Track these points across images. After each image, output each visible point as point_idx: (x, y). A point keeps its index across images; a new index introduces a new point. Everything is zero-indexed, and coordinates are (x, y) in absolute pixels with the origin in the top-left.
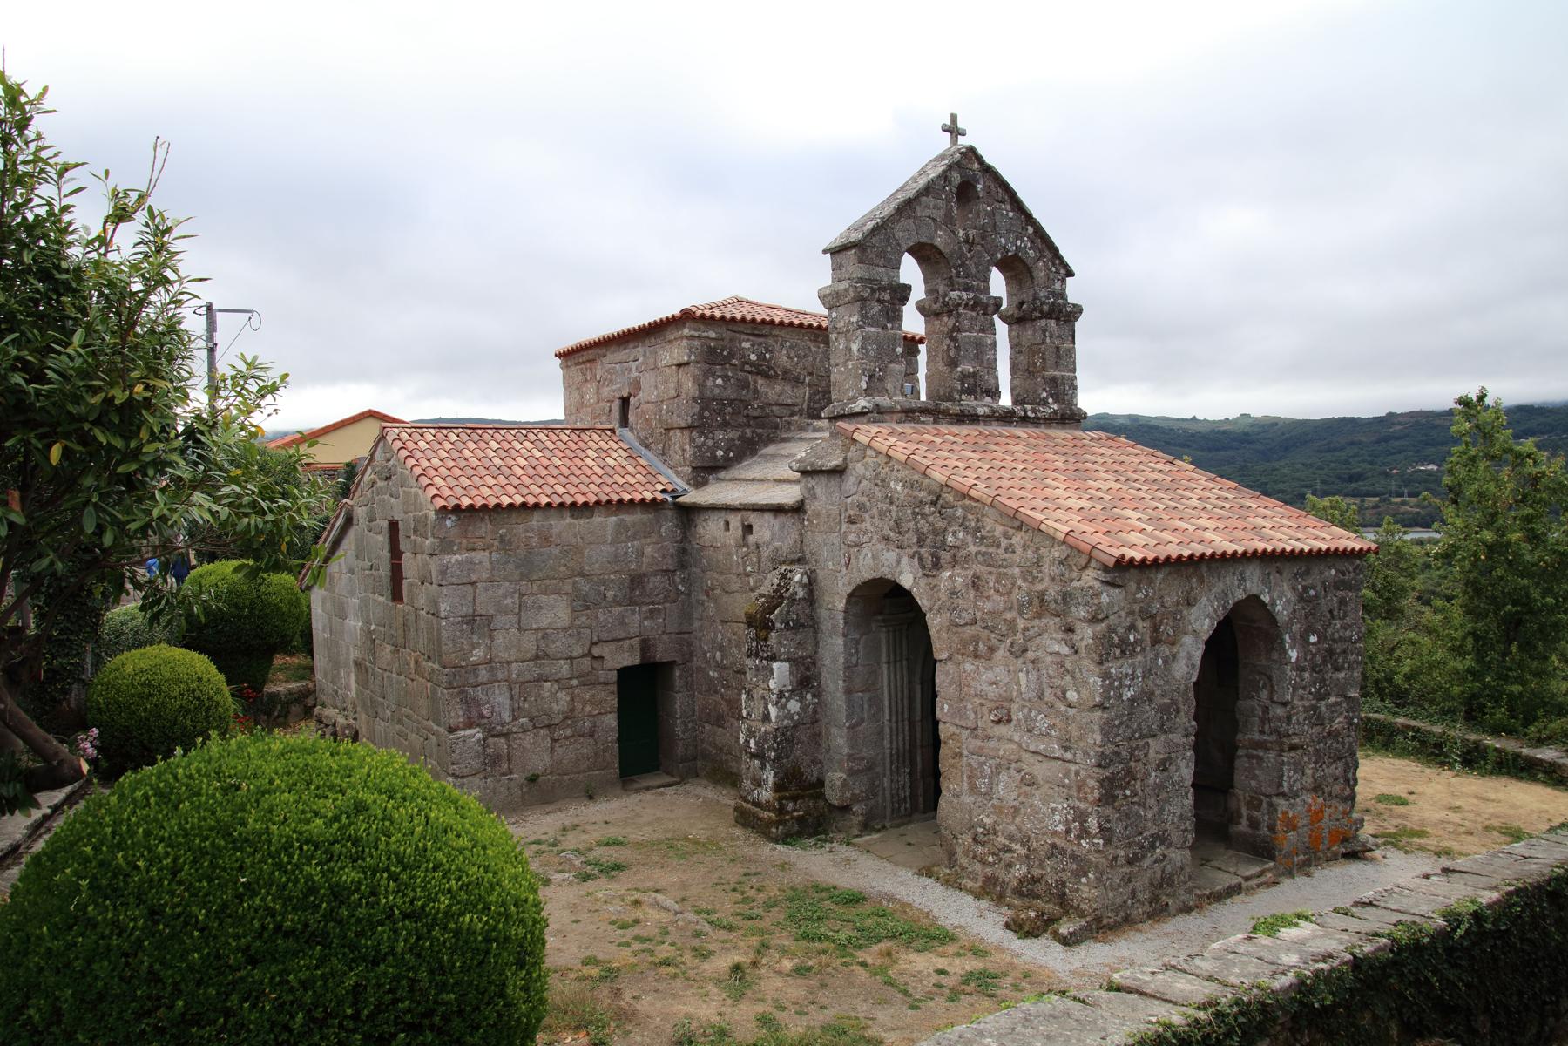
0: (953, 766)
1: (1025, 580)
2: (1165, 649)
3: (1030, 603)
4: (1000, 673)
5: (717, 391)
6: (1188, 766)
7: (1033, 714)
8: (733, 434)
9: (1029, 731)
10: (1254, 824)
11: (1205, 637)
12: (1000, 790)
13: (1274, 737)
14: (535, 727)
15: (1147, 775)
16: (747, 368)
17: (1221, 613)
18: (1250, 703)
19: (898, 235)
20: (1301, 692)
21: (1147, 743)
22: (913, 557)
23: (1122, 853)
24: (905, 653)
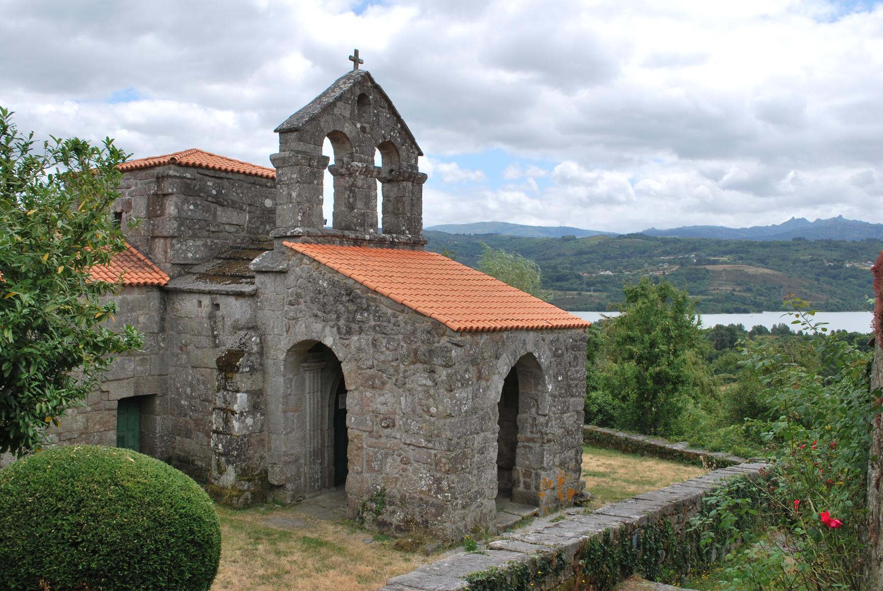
0: (357, 455)
1: (406, 342)
2: (483, 383)
3: (408, 355)
4: (388, 397)
5: (190, 213)
6: (494, 451)
7: (409, 421)
8: (199, 243)
9: (406, 432)
10: (527, 486)
11: (505, 377)
12: (388, 469)
13: (538, 435)
14: (60, 440)
15: (473, 456)
16: (210, 199)
17: (513, 363)
18: (525, 415)
19: (322, 124)
20: (553, 409)
21: (474, 437)
22: (333, 327)
23: (460, 502)
24: (319, 387)
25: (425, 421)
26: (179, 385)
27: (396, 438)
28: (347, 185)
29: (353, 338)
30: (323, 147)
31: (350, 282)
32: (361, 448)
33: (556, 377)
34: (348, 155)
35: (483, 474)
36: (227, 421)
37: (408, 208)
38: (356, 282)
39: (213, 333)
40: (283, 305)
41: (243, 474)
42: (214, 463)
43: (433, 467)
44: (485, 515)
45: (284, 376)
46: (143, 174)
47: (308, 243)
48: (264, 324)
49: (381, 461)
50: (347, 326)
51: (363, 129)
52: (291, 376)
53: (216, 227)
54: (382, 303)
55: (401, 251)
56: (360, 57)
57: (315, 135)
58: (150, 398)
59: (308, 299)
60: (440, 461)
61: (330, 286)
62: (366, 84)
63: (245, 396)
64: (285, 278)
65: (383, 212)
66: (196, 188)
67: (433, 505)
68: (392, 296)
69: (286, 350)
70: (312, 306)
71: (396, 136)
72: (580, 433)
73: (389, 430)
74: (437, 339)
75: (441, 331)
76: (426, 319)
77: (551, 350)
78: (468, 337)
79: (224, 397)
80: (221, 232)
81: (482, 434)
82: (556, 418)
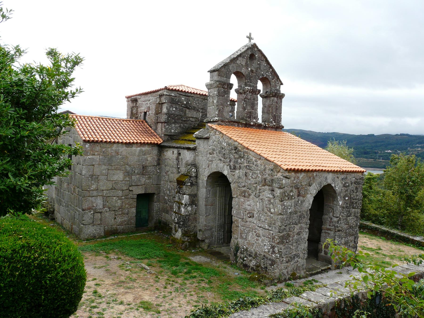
1: (261, 175)
2: (301, 198)
4: (251, 202)
5: (173, 112)
6: (306, 234)
7: (261, 215)
8: (177, 125)
9: (259, 220)
10: (326, 253)
11: (314, 196)
13: (333, 227)
14: (110, 211)
15: (294, 236)
16: (183, 106)
17: (319, 189)
19: (230, 68)
20: (342, 214)
21: (294, 226)
22: (228, 166)
23: (285, 259)
25: (268, 216)
26: (164, 190)
27: (254, 223)
28: (243, 98)
29: (236, 172)
30: (231, 79)
31: (236, 143)
32: (238, 226)
33: (344, 197)
34: (244, 84)
35: (299, 246)
36: (179, 208)
37: (274, 110)
38: (239, 143)
39: (178, 166)
40: (207, 154)
41: (185, 234)
42: (173, 227)
43: (271, 240)
44: (299, 267)
45: (206, 188)
46: (155, 94)
47: (221, 125)
48: (198, 163)
49: (247, 234)
50: (234, 165)
51: (252, 71)
52: (210, 189)
53: (186, 119)
54: (251, 154)
55: (270, 131)
56: (252, 37)
57: (227, 73)
58: (152, 195)
59: (218, 151)
60: (275, 237)
61: (227, 145)
62: (254, 49)
63: (188, 196)
64: (208, 142)
65: (263, 112)
66: (176, 101)
67: (270, 260)
68: (255, 151)
69: (207, 176)
70: (219, 155)
71: (269, 75)
72: (357, 228)
73: (251, 219)
74: (276, 174)
75: (278, 170)
76: (271, 163)
77: (342, 183)
78: (293, 174)
79: (179, 196)
80: (188, 121)
81: (299, 225)
82: (343, 219)
